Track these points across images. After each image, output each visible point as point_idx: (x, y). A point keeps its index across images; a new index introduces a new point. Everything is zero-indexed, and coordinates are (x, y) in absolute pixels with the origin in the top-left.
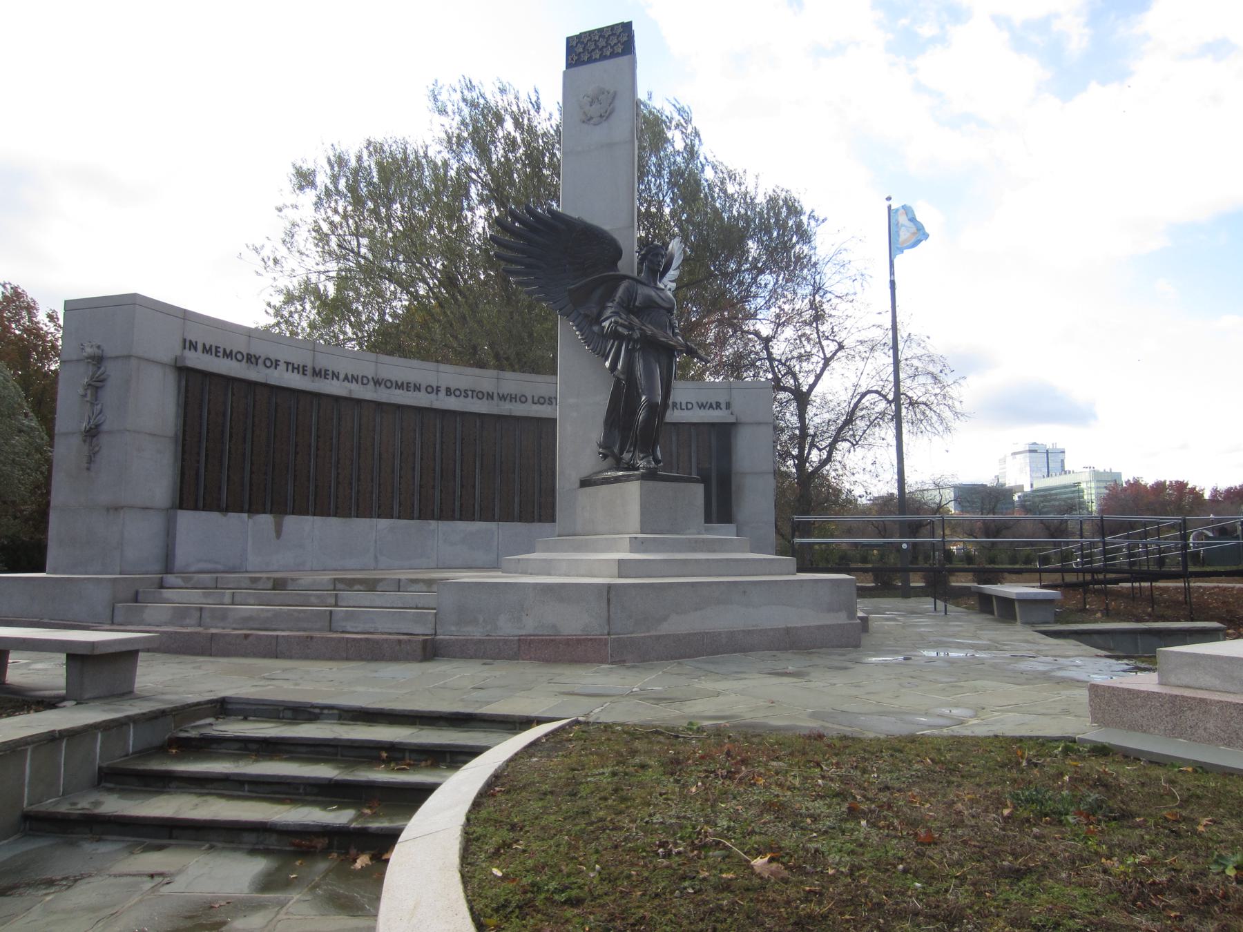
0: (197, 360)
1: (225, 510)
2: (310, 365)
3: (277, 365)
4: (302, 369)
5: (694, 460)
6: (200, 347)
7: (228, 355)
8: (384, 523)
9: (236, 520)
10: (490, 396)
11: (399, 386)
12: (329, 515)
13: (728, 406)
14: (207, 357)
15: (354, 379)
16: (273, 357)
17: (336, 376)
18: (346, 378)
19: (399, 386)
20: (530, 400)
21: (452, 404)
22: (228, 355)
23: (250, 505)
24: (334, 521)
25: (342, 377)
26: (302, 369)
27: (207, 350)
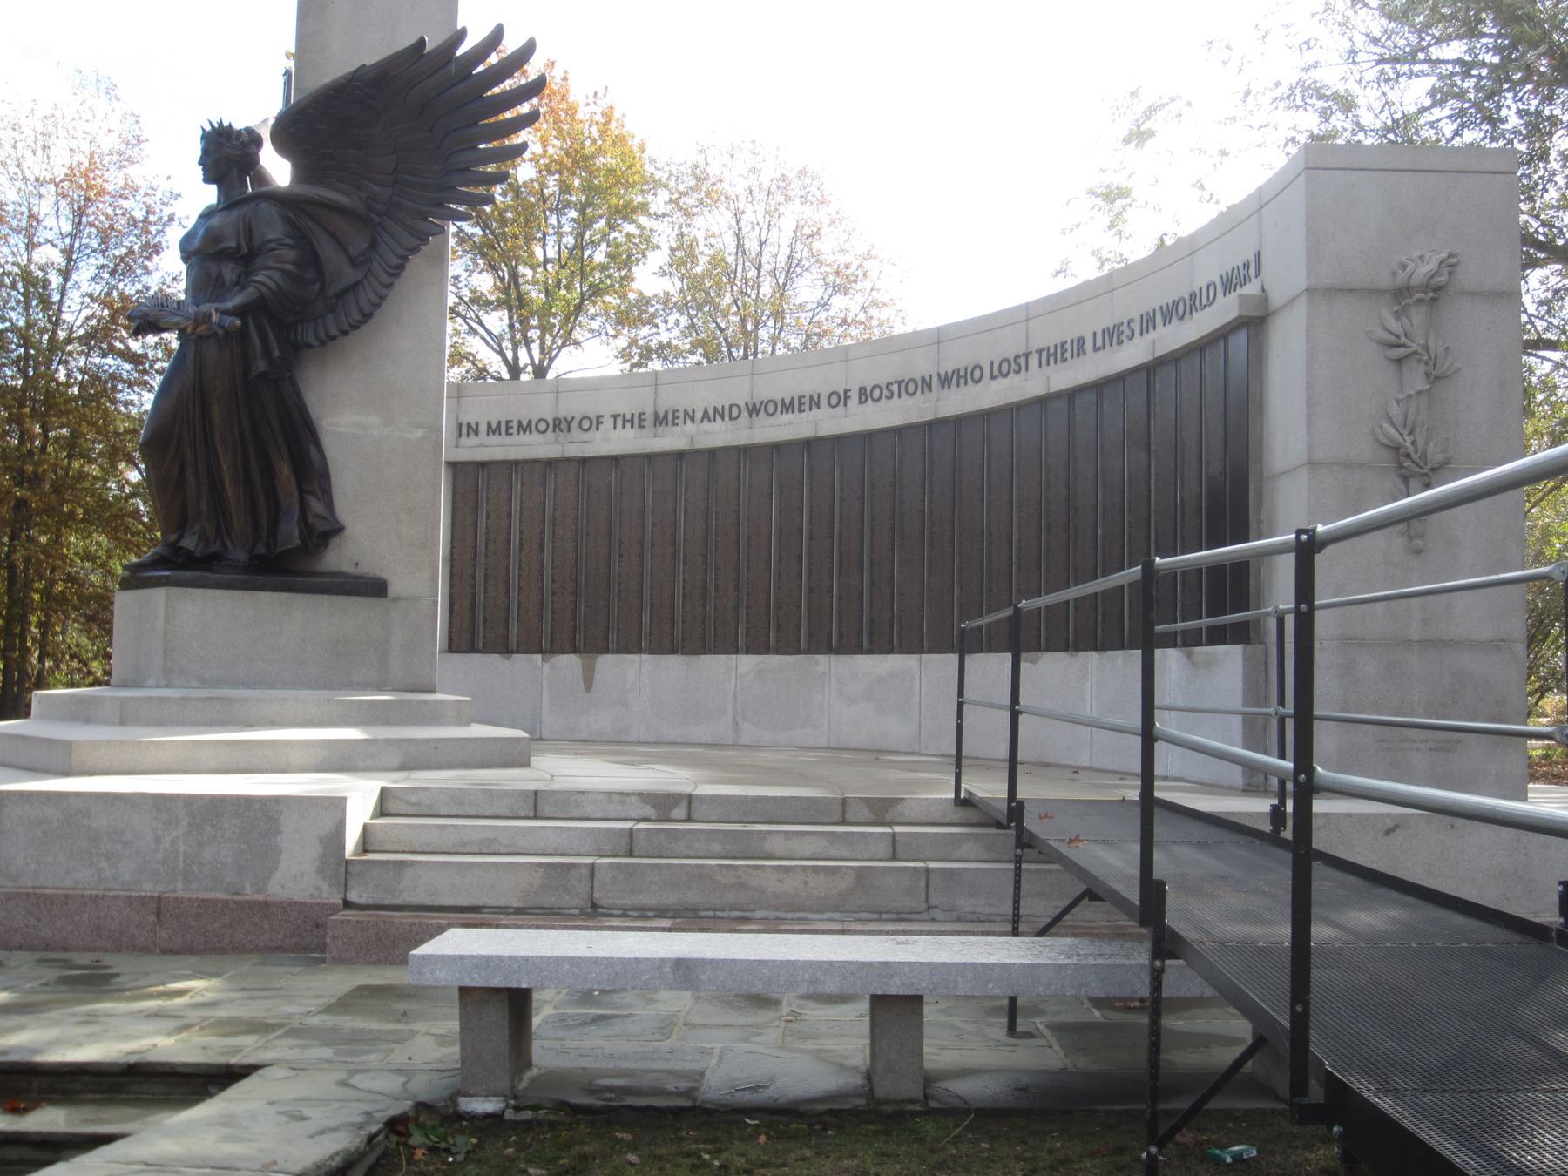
1: (506, 650)
2: (649, 410)
3: (599, 423)
7: (525, 428)
8: (747, 663)
9: (525, 664)
10: (926, 384)
11: (787, 407)
17: (690, 416)
18: (706, 415)
19: (787, 407)
22: (525, 428)
24: (673, 662)
25: (698, 416)
27: (493, 430)
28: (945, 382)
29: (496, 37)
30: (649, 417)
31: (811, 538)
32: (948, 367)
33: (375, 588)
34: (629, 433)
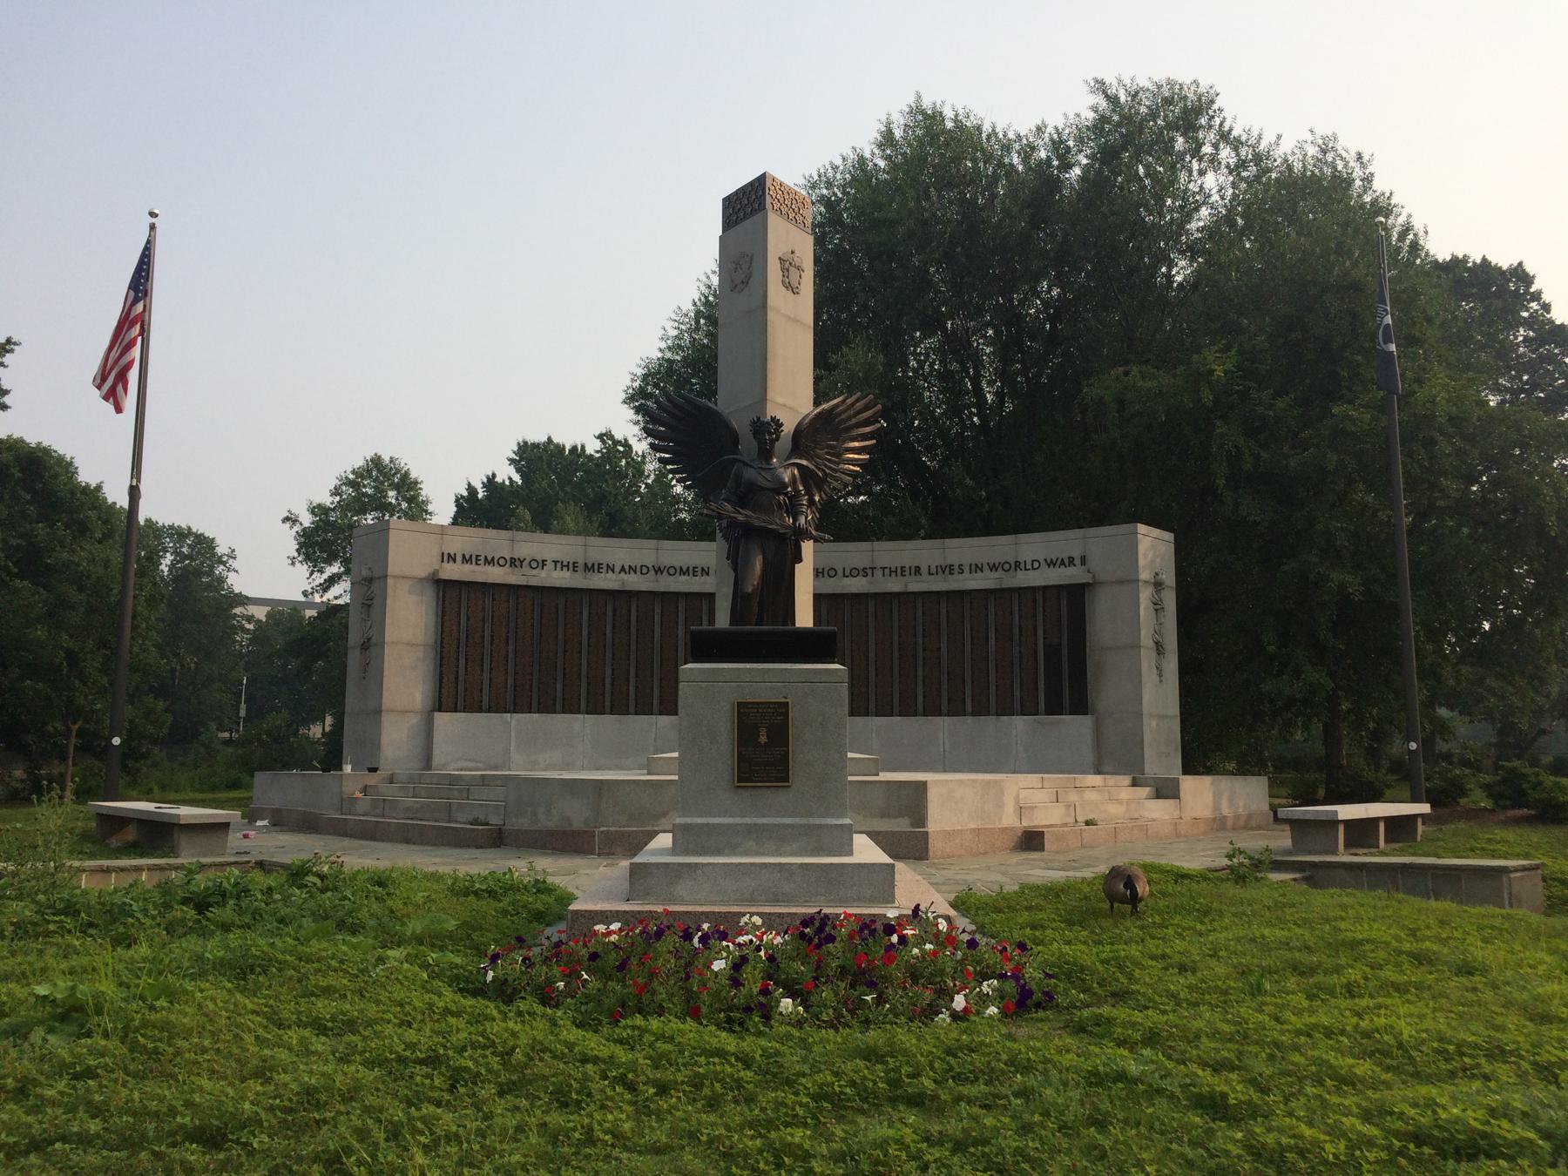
0: (453, 571)
2: (581, 562)
4: (573, 567)
5: (1040, 632)
6: (459, 558)
7: (490, 562)
11: (683, 572)
12: (603, 713)
13: (1083, 560)
14: (467, 567)
15: (632, 569)
16: (539, 558)
17: (610, 568)
18: (623, 569)
19: (683, 572)
20: (840, 573)
21: (894, 585)
23: (515, 704)
24: (609, 720)
25: (617, 569)
26: (573, 567)
27: (465, 560)
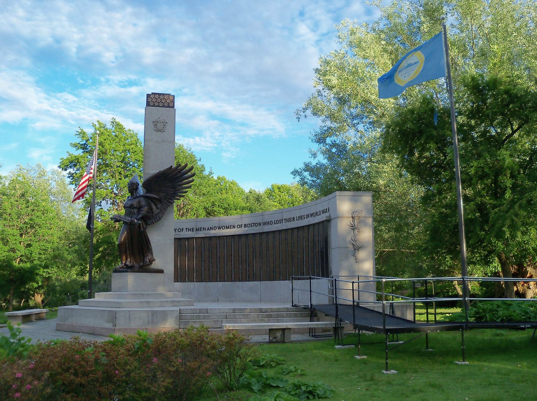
8: (220, 284)
10: (260, 224)
18: (208, 229)
28: (264, 224)
29: (186, 165)
30: (195, 229)
31: (234, 256)
32: (265, 221)
33: (161, 271)
34: (190, 233)
